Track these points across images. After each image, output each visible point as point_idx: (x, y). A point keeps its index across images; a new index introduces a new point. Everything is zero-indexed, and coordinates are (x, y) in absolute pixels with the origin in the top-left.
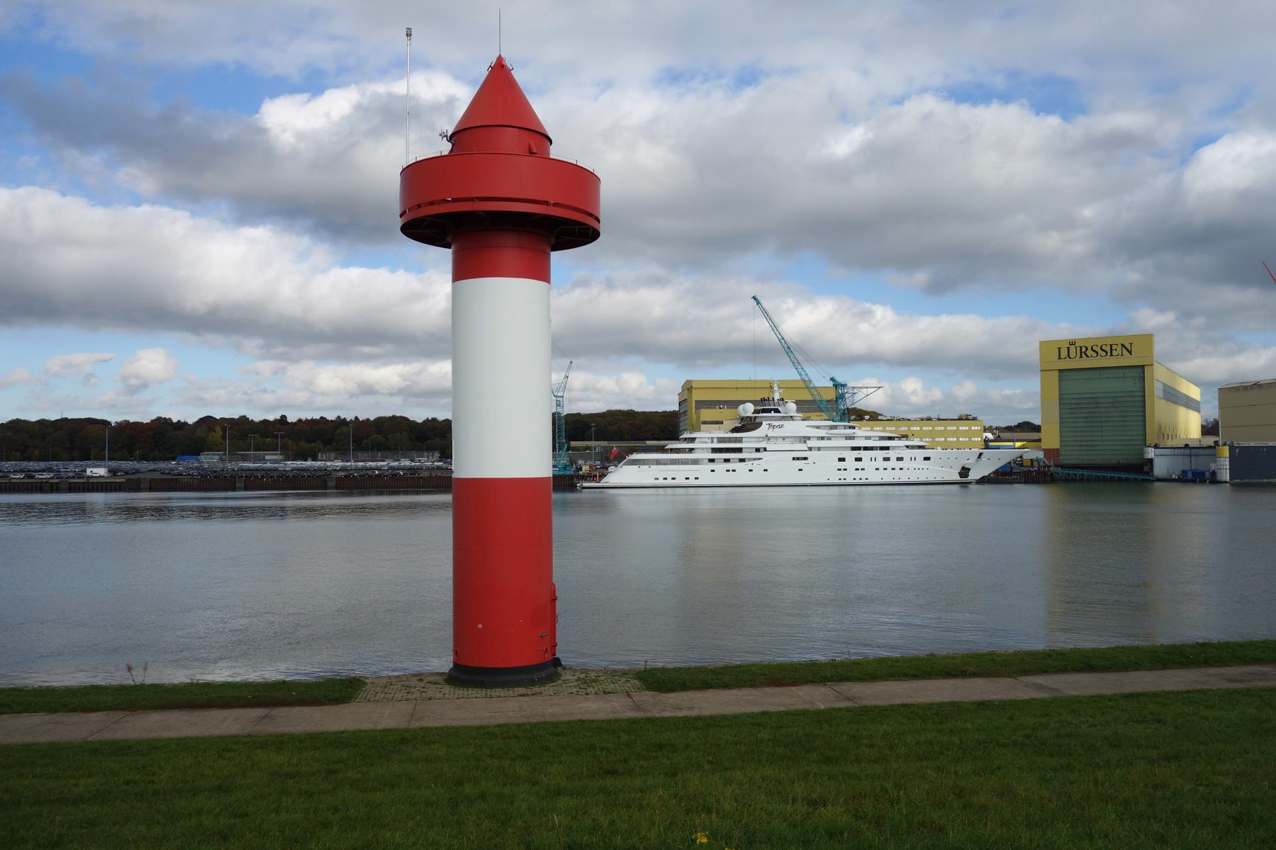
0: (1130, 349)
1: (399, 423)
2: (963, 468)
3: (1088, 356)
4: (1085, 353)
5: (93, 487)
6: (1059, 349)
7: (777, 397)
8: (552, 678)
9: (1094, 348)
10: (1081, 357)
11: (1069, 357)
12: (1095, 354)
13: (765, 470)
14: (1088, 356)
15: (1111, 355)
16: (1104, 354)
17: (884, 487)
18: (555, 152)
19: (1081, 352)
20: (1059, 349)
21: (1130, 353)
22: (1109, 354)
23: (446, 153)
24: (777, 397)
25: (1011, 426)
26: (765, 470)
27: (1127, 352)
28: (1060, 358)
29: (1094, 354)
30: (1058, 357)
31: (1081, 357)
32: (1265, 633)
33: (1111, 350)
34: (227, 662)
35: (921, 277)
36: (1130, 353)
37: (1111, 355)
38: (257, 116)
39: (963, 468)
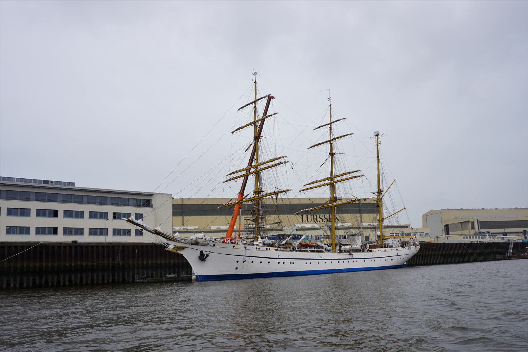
4: (316, 219)
19: (314, 219)
22: (328, 220)
28: (302, 222)
33: (329, 218)
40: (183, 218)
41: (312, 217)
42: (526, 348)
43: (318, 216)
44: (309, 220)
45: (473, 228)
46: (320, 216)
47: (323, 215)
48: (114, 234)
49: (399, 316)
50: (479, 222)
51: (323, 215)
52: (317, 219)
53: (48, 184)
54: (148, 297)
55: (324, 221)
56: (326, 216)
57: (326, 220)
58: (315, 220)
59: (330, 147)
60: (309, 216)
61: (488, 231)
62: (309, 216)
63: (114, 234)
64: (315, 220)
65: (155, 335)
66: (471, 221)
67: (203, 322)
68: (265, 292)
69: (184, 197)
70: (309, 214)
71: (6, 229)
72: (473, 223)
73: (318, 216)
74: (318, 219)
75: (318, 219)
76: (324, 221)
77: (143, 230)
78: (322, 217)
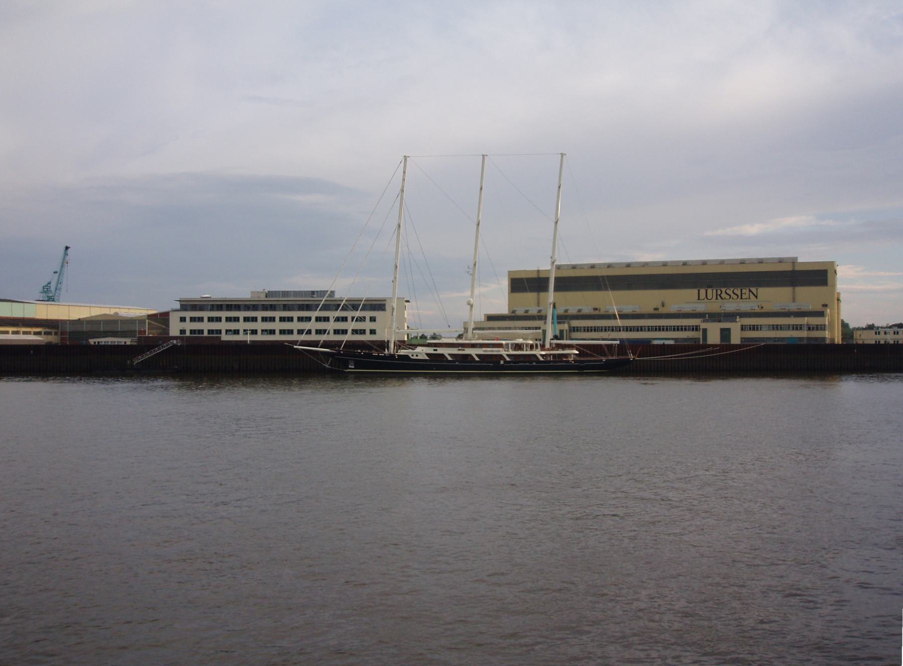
0: (756, 295)
1: (644, 347)
2: (375, 330)
3: (722, 299)
4: (720, 295)
5: (757, 328)
9: (736, 297)
10: (717, 299)
11: (707, 299)
12: (728, 297)
14: (722, 299)
15: (741, 298)
16: (735, 297)
18: (792, 316)
21: (756, 297)
22: (740, 297)
25: (794, 317)
27: (753, 295)
28: (699, 299)
29: (728, 297)
30: (697, 298)
31: (717, 299)
32: (473, 317)
33: (741, 294)
35: (234, 399)
36: (756, 297)
37: (741, 298)
38: (609, 289)
39: (375, 330)
40: (538, 294)
41: (715, 291)
42: (825, 654)
43: (724, 290)
44: (709, 296)
46: (733, 291)
47: (732, 289)
48: (364, 318)
50: (266, 299)
52: (722, 295)
54: (752, 580)
56: (736, 291)
57: (736, 297)
60: (710, 291)
62: (710, 291)
63: (364, 318)
68: (690, 477)
69: (540, 269)
73: (724, 290)
74: (723, 295)
75: (723, 295)
76: (733, 298)
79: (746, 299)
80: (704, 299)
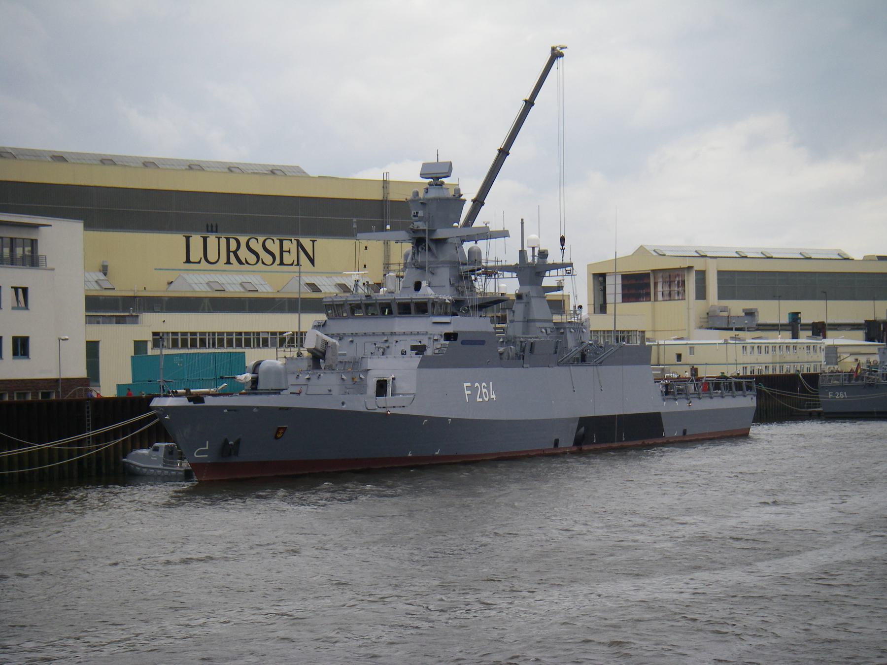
3: (240, 262)
6: (556, 55)
7: (709, 492)
8: (483, 344)
10: (228, 262)
13: (366, 247)
14: (240, 262)
15: (282, 263)
16: (268, 259)
17: (782, 257)
19: (228, 251)
20: (556, 55)
21: (312, 261)
22: (278, 261)
23: (247, 365)
24: (709, 492)
26: (366, 247)
28: (188, 261)
29: (252, 259)
30: (185, 260)
31: (228, 262)
33: (282, 252)
34: (20, 622)
36: (312, 261)
41: (223, 242)
43: (243, 240)
44: (212, 257)
45: (701, 293)
47: (261, 239)
49: (205, 657)
51: (261, 239)
53: (720, 273)
55: (263, 263)
56: (269, 244)
58: (232, 255)
59: (547, 61)
60: (212, 240)
61: (748, 307)
62: (212, 240)
64: (232, 255)
65: (622, 543)
66: (696, 268)
67: (130, 610)
70: (212, 231)
71: (275, 331)
72: (701, 276)
73: (243, 240)
74: (243, 253)
75: (243, 253)
76: (263, 263)
77: (494, 331)
78: (256, 246)
79: (292, 265)
80: (199, 262)
